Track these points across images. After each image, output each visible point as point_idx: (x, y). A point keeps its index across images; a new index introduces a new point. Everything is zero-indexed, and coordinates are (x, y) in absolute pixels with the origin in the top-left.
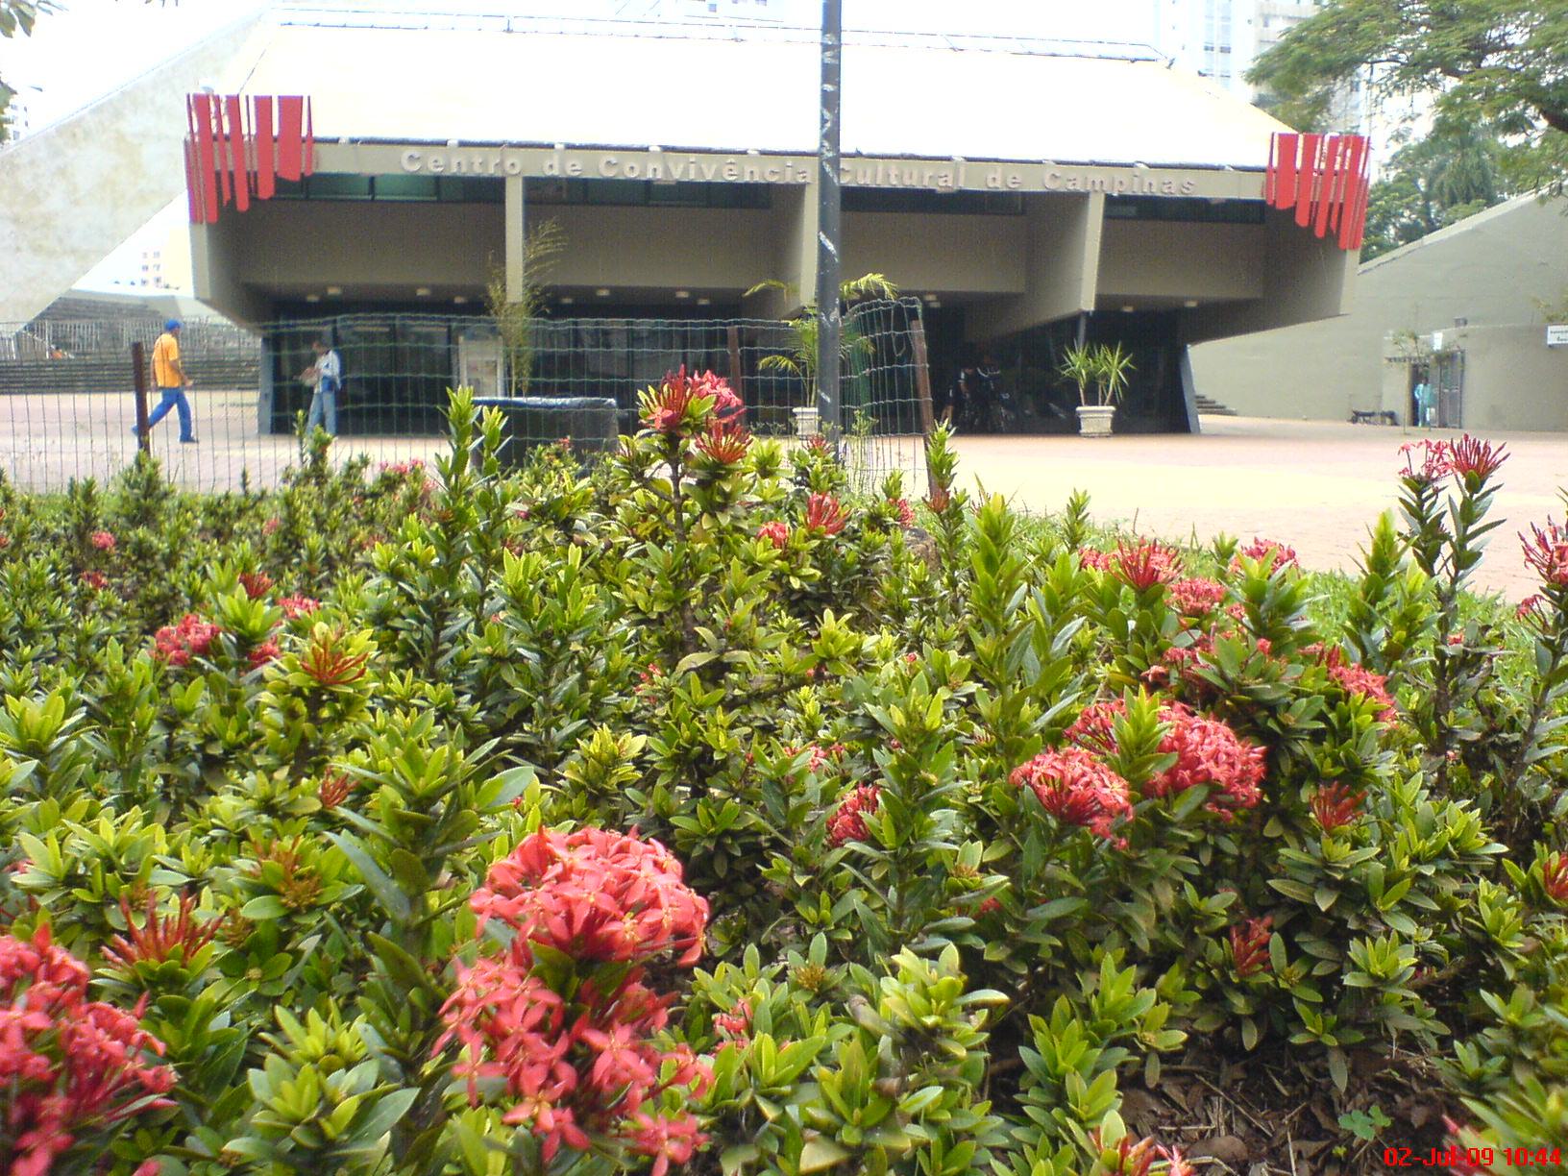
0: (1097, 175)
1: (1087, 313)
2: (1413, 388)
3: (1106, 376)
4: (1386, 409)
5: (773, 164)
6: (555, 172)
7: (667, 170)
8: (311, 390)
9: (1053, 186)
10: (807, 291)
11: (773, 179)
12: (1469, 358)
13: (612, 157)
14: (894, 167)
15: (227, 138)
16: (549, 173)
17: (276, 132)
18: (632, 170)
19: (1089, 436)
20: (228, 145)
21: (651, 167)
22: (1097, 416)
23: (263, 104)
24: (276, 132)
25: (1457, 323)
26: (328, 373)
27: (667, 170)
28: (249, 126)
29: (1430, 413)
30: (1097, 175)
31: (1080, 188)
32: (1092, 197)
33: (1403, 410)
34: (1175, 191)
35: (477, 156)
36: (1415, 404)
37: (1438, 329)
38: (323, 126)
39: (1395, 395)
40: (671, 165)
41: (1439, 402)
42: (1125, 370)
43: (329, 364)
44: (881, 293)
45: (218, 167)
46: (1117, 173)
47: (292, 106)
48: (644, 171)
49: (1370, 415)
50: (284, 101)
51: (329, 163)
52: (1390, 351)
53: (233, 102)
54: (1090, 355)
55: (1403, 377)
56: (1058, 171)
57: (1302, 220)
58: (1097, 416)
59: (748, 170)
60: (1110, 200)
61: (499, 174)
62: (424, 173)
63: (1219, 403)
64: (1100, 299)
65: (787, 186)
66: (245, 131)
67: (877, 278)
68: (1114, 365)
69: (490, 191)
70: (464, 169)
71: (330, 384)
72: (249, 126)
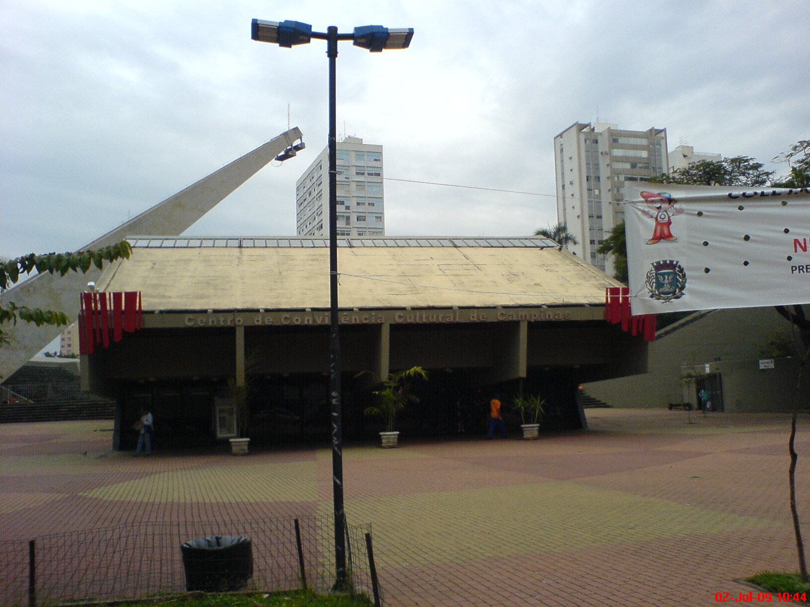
0: (523, 312)
1: (523, 378)
2: (698, 391)
3: (534, 409)
4: (686, 401)
5: (365, 315)
6: (260, 323)
7: (314, 320)
8: (139, 431)
9: (501, 318)
10: (384, 373)
11: (366, 322)
12: (724, 378)
13: (287, 315)
14: (424, 314)
15: (99, 312)
16: (257, 324)
17: (123, 308)
18: (297, 320)
19: (528, 439)
20: (100, 316)
21: (306, 318)
22: (531, 429)
23: (117, 296)
24: (123, 308)
25: (716, 359)
26: (146, 423)
27: (314, 320)
28: (110, 306)
29: (708, 405)
30: (523, 312)
31: (515, 318)
32: (521, 323)
33: (694, 402)
34: (561, 318)
35: (221, 317)
36: (699, 399)
37: (707, 362)
38: (146, 304)
39: (690, 395)
40: (316, 317)
41: (712, 398)
42: (543, 406)
43: (148, 419)
44: (420, 375)
45: (95, 327)
46: (533, 311)
47: (132, 297)
48: (303, 320)
49: (679, 405)
50: (127, 294)
51: (150, 323)
52: (685, 373)
53: (103, 295)
54: (525, 399)
55: (693, 388)
56: (504, 311)
57: (625, 328)
58: (531, 429)
59: (353, 318)
60: (529, 323)
61: (233, 325)
62: (196, 326)
63: (603, 401)
64: (529, 370)
65: (373, 325)
66: (108, 308)
67: (418, 369)
68: (538, 405)
69: (230, 331)
70: (215, 323)
71: (148, 428)
72: (110, 306)
